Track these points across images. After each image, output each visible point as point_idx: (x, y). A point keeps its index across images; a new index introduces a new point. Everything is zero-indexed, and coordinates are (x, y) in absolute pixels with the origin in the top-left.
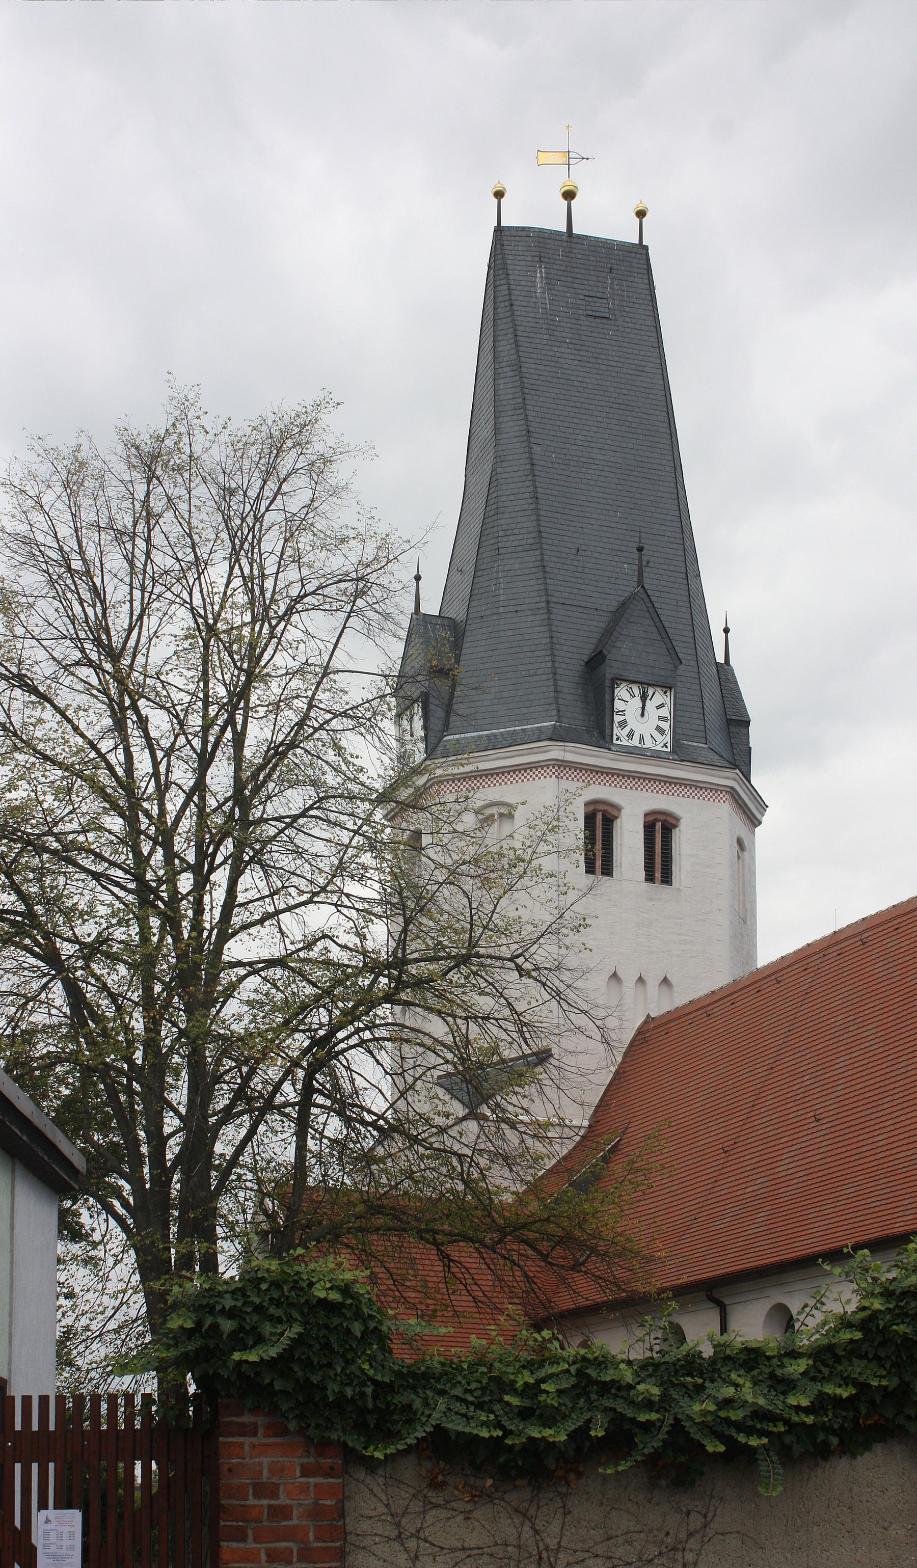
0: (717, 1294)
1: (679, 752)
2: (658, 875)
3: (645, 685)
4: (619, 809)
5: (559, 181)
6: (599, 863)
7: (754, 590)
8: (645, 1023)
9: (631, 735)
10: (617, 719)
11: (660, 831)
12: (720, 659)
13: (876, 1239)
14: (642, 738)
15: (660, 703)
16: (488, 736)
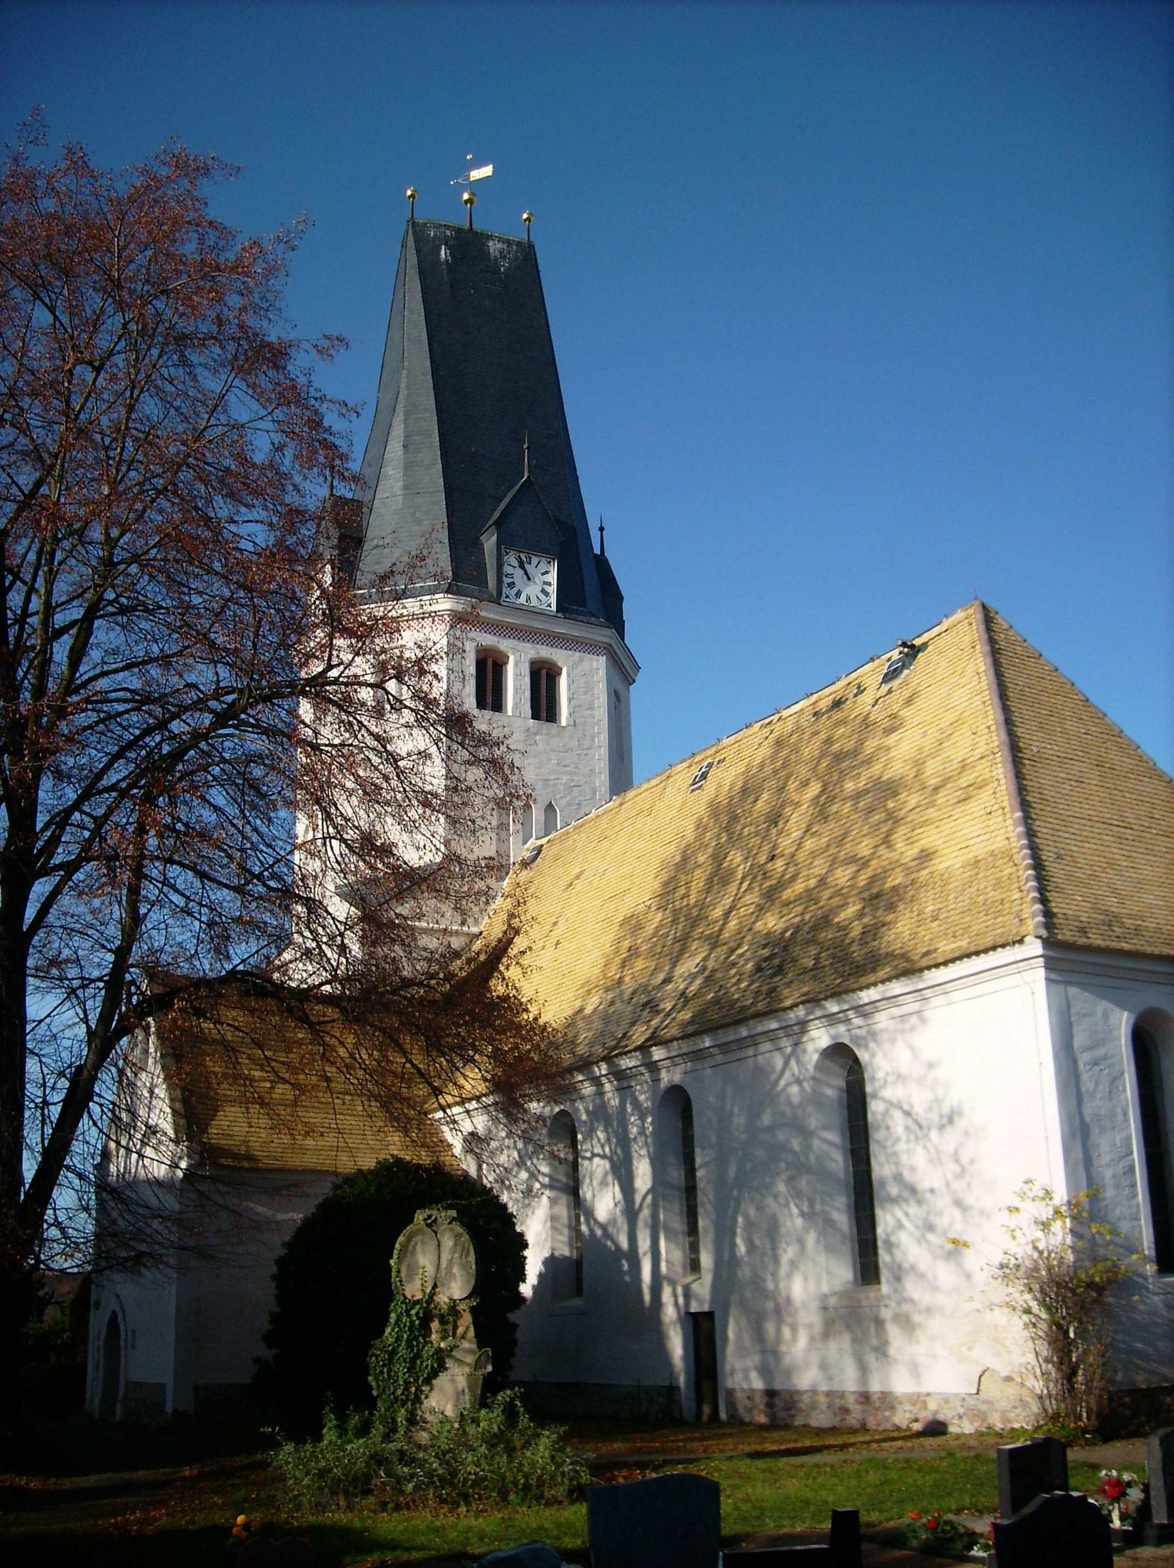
9: (518, 594)
11: (543, 680)
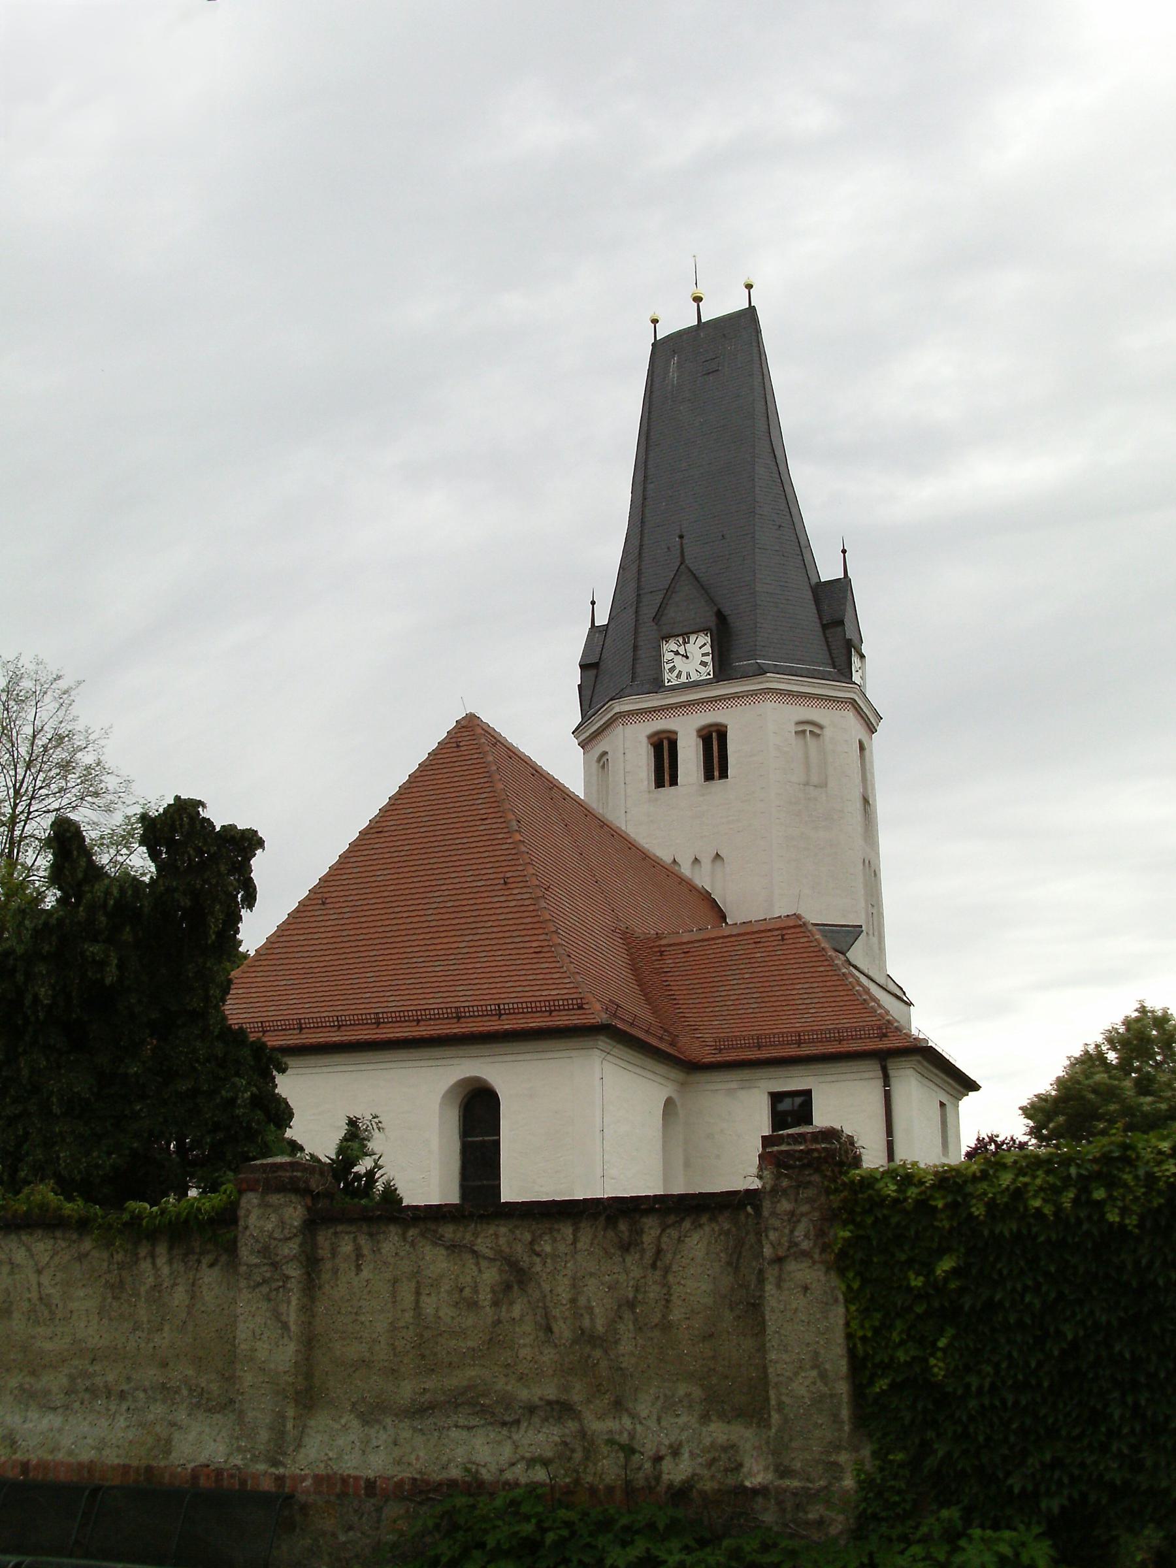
2: (716, 774)
4: (676, 733)
6: (667, 777)
7: (838, 503)
9: (679, 675)
10: (667, 667)
11: (715, 744)
13: (489, 1031)
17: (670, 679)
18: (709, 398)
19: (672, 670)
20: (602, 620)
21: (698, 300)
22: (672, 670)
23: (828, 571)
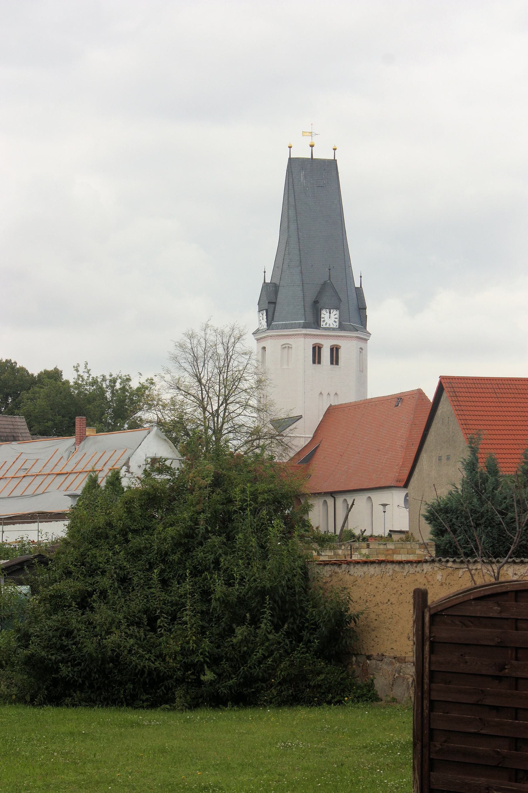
0: (333, 495)
1: (341, 327)
2: (334, 363)
3: (330, 308)
5: (308, 140)
6: (317, 361)
7: (366, 259)
8: (330, 406)
9: (326, 324)
10: (322, 320)
11: (335, 351)
12: (357, 285)
14: (329, 324)
15: (335, 314)
16: (285, 324)
17: (323, 324)
18: (313, 189)
19: (324, 321)
20: (268, 280)
21: (312, 146)
22: (324, 321)
23: (357, 285)
